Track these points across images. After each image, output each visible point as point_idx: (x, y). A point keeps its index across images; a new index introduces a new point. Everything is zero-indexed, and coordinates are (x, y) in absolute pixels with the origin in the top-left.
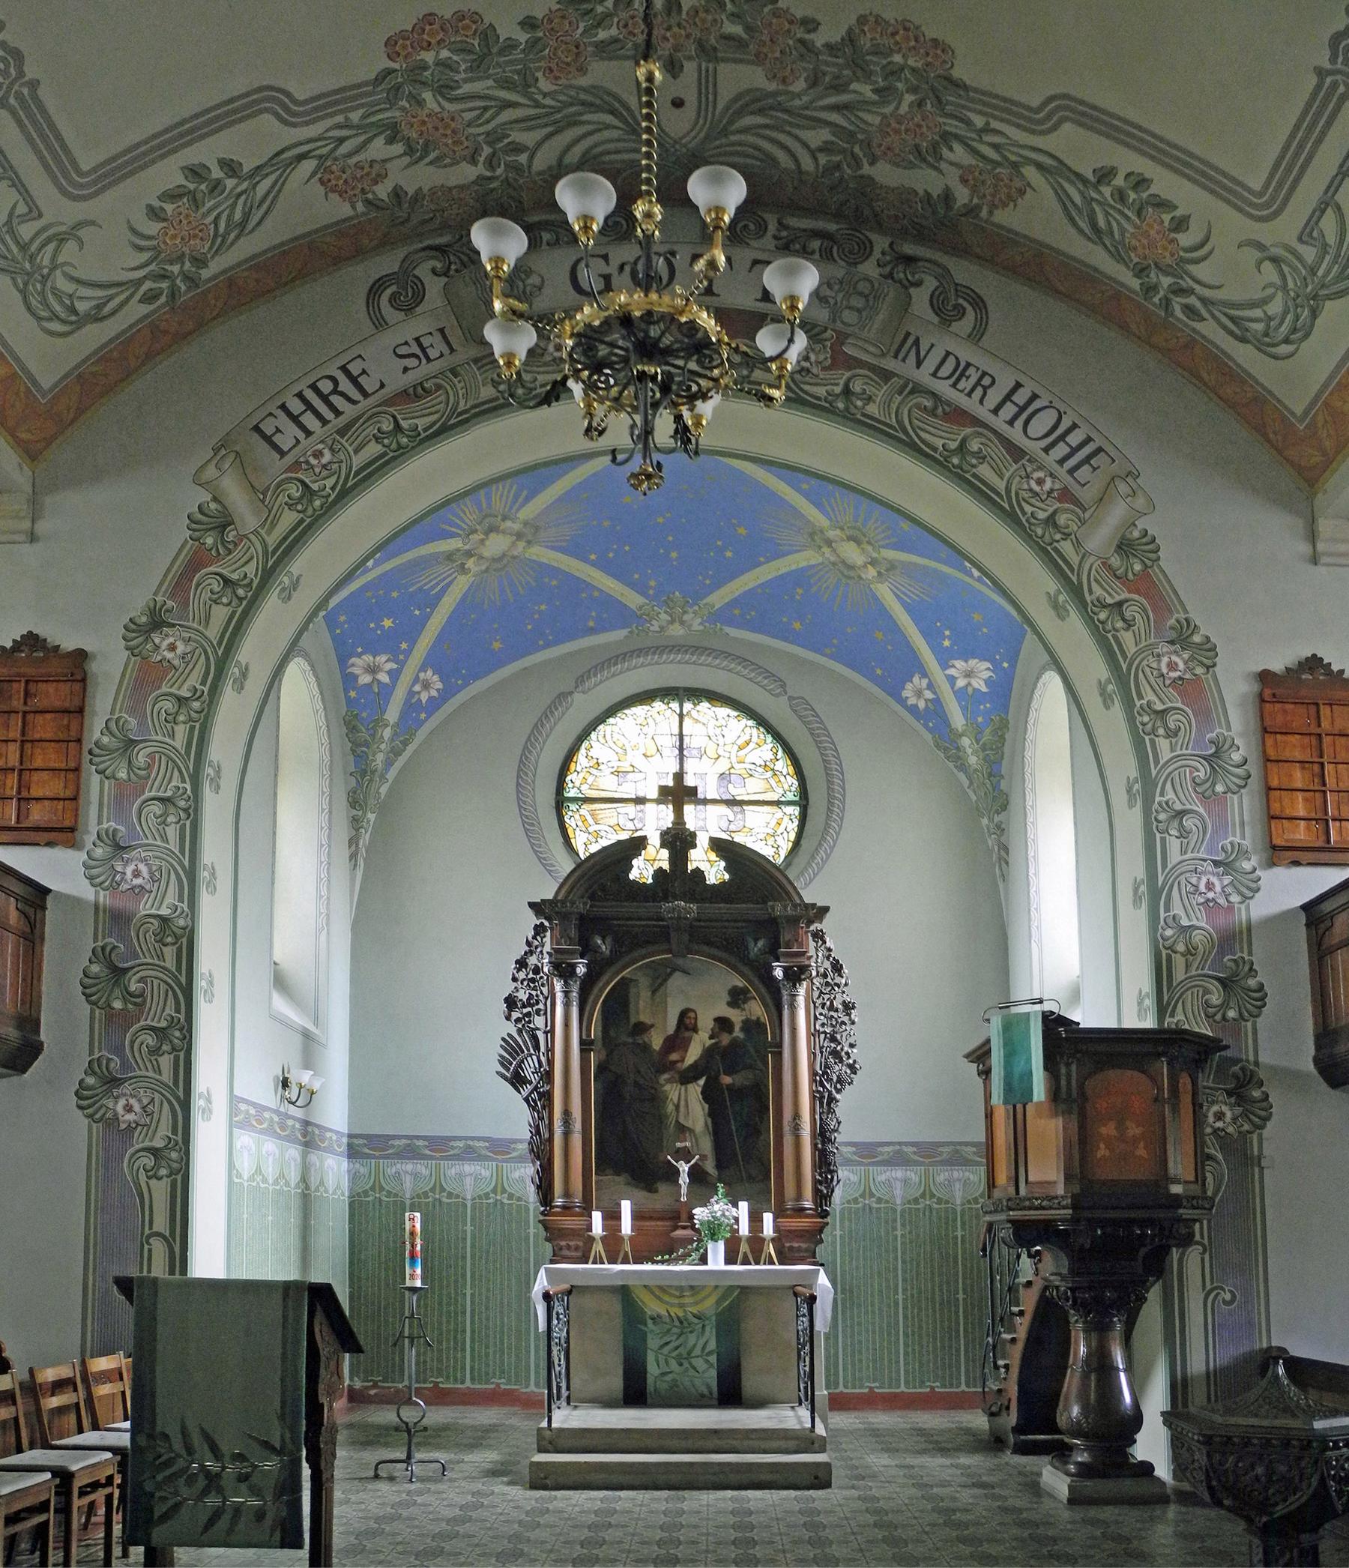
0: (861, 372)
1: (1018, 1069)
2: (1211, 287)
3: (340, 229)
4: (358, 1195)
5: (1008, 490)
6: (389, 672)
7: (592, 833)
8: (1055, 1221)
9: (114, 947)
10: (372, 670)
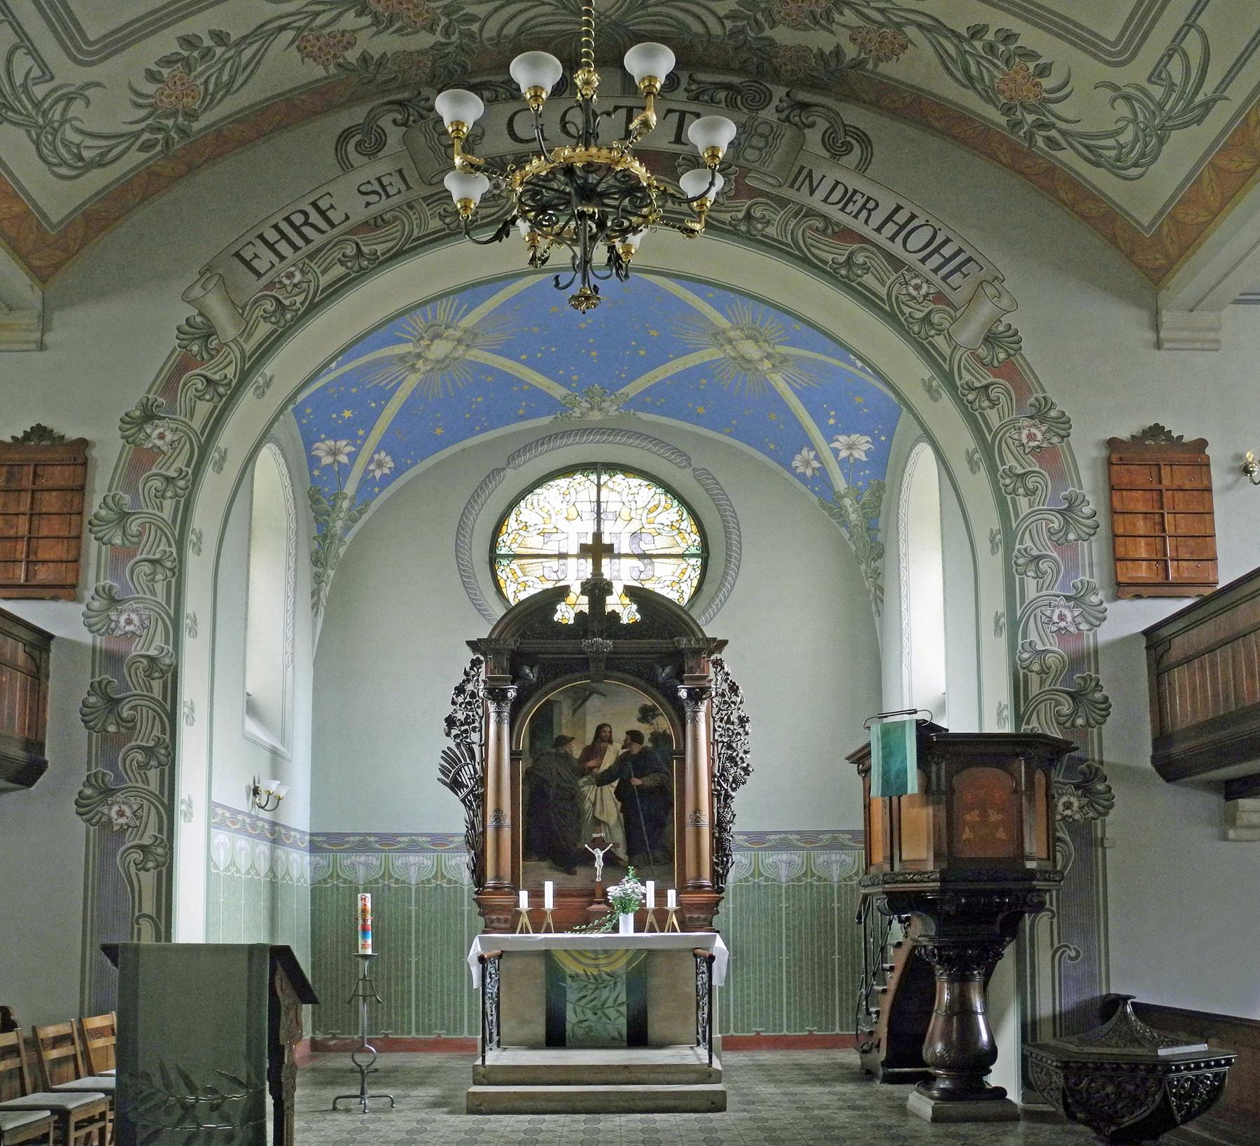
0: (763, 200)
1: (895, 767)
2: (1067, 121)
3: (312, 89)
4: (319, 882)
5: (889, 295)
6: (348, 455)
7: (522, 584)
8: (925, 892)
9: (109, 682)
10: (334, 453)
